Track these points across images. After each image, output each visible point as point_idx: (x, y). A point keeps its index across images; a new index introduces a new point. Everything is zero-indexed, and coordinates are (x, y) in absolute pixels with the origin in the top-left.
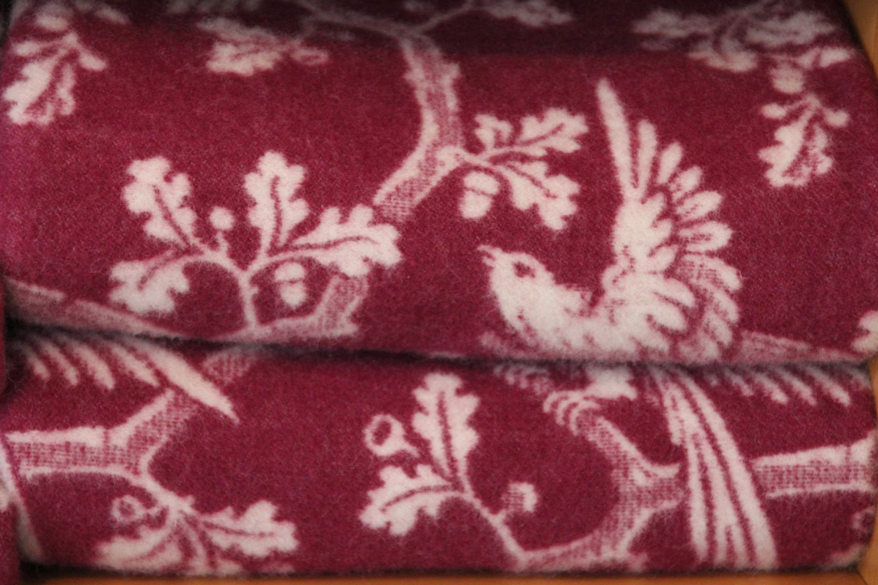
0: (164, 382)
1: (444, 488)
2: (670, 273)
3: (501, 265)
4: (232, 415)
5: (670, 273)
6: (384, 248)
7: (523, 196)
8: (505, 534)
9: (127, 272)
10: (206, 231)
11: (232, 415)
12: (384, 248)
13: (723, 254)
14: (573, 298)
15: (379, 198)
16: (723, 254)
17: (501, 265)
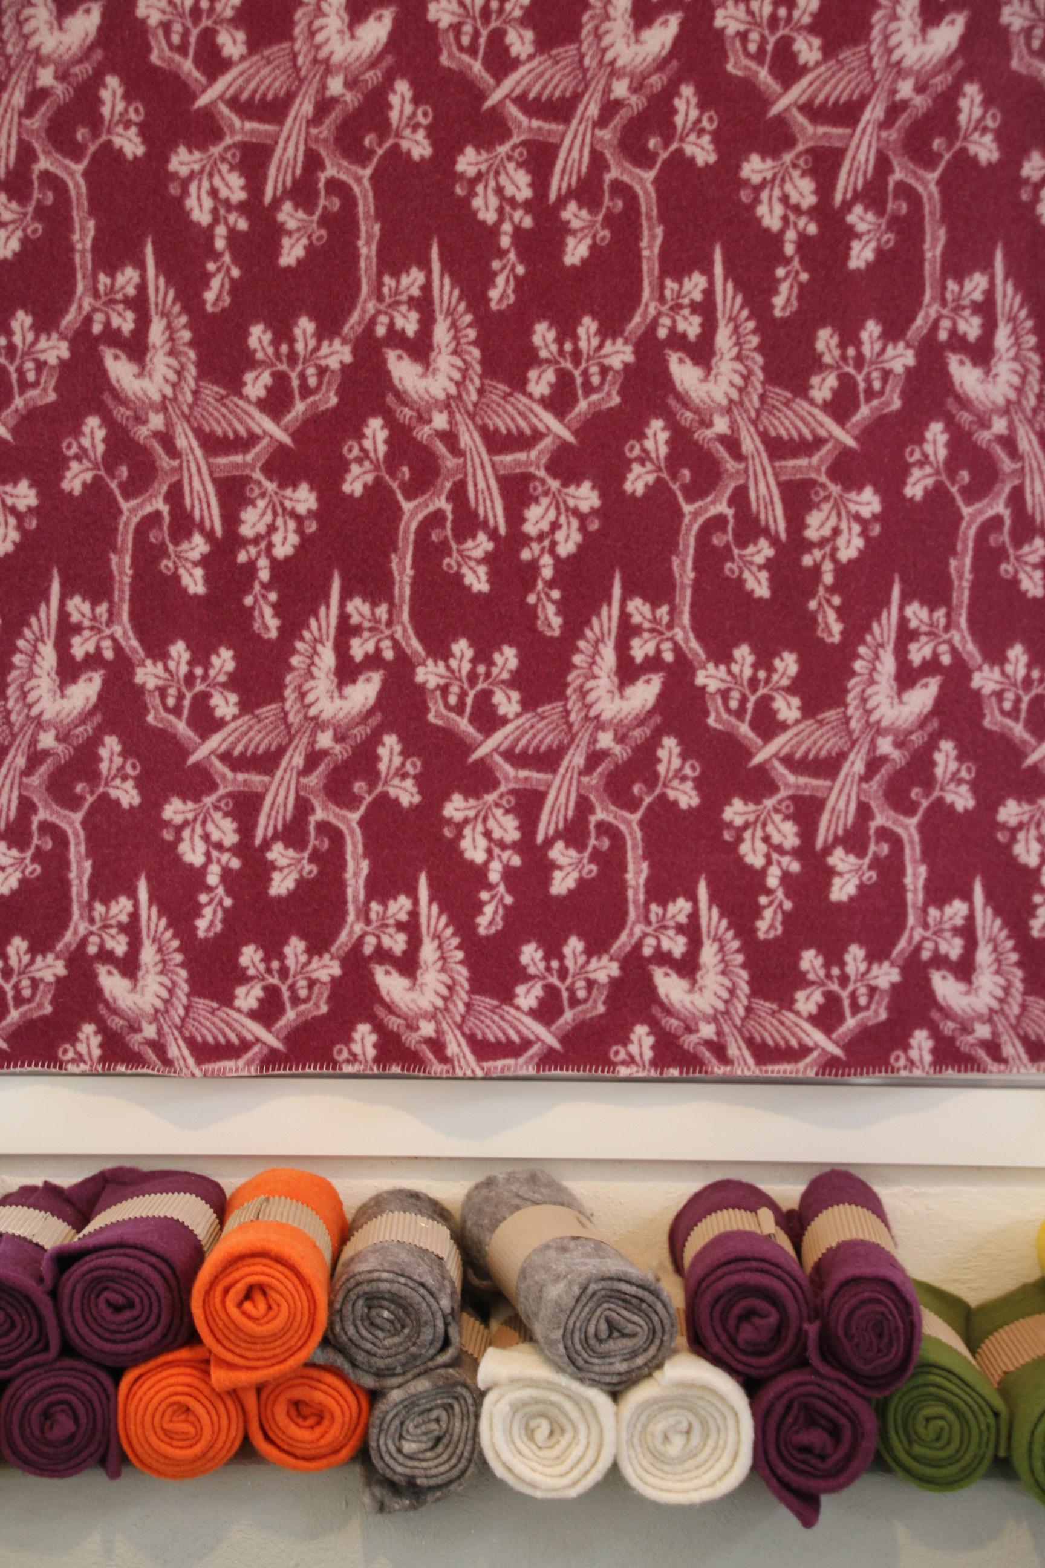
0: (831, 436)
1: (41, 1280)
2: (162, 972)
3: (102, 970)
4: (1000, 245)
5: (162, 972)
6: (614, 970)
7: (666, 945)
8: (449, 525)
9: (240, 991)
10: (269, 970)
11: (1000, 245)
12: (614, 970)
13: (461, 962)
14: (961, 987)
15: (612, 951)
16: (461, 962)
17: (102, 970)
